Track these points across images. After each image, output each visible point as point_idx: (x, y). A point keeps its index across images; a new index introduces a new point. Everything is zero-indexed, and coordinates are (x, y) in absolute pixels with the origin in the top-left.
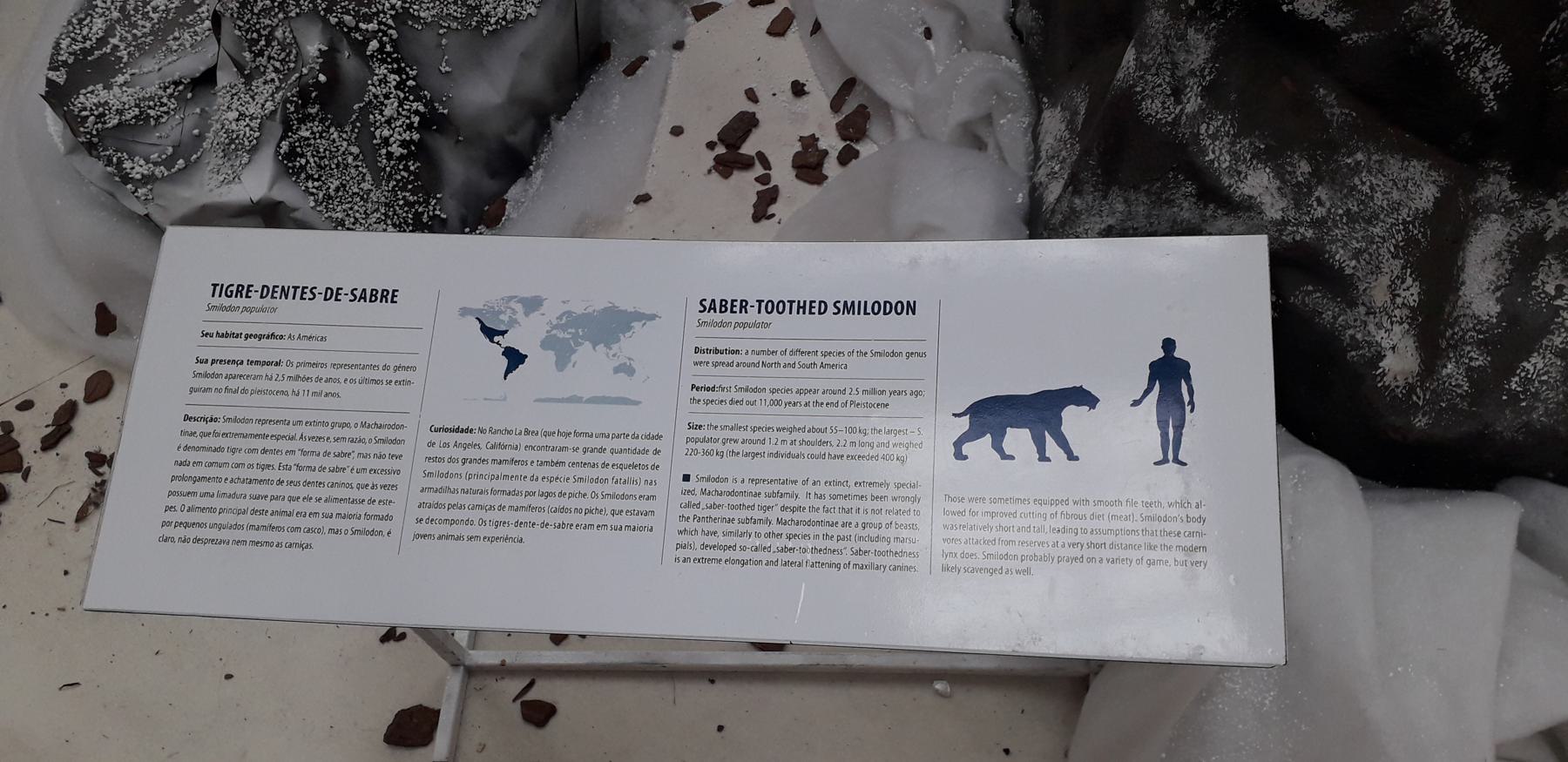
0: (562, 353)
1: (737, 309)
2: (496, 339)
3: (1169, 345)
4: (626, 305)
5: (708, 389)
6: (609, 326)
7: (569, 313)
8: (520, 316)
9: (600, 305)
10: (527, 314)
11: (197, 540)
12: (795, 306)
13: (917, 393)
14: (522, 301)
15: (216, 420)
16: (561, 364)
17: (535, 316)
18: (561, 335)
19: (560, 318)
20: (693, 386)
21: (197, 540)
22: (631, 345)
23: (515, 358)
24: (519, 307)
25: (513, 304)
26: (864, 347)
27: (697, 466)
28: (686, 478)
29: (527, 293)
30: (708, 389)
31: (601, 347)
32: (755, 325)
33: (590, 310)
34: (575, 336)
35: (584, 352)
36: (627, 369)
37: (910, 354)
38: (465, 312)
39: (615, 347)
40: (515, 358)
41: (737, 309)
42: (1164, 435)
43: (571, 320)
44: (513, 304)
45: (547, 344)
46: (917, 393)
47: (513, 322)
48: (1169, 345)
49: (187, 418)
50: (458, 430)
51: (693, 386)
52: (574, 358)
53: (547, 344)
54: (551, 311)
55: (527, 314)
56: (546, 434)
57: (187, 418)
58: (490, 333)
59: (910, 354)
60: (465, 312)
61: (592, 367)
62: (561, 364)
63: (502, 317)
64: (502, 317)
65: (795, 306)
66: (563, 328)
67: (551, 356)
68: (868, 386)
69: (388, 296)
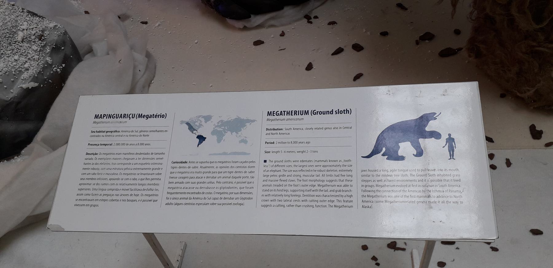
0: (219, 135)
1: (293, 114)
2: (194, 132)
3: (450, 135)
4: (243, 117)
5: (271, 143)
6: (237, 125)
7: (222, 121)
8: (203, 123)
9: (233, 117)
10: (206, 122)
11: (128, 201)
12: (286, 113)
13: (166, 131)
14: (204, 117)
15: (97, 154)
16: (219, 141)
17: (209, 122)
18: (219, 129)
19: (218, 123)
20: (266, 142)
21: (128, 201)
22: (245, 132)
23: (201, 139)
24: (203, 120)
25: (200, 118)
26: (336, 126)
27: (267, 157)
28: (265, 161)
29: (205, 114)
30: (271, 143)
31: (234, 133)
32: (106, 123)
33: (230, 119)
34: (224, 129)
35: (229, 136)
36: (244, 141)
37: (326, 129)
38: (182, 122)
39: (240, 133)
40: (201, 139)
41: (293, 114)
42: (450, 153)
43: (222, 123)
44: (200, 118)
45: (214, 133)
46: (166, 131)
47: (201, 125)
48: (450, 135)
49: (87, 154)
50: (182, 162)
51: (266, 142)
52: (224, 138)
53: (214, 133)
54: (215, 120)
55: (206, 122)
56: (211, 162)
57: (87, 154)
58: (191, 129)
59: (326, 129)
60: (182, 122)
61: (231, 140)
62: (219, 141)
63: (196, 124)
64: (196, 124)
65: (286, 113)
66: (220, 127)
67: (215, 137)
68: (140, 129)
69: (347, 111)
